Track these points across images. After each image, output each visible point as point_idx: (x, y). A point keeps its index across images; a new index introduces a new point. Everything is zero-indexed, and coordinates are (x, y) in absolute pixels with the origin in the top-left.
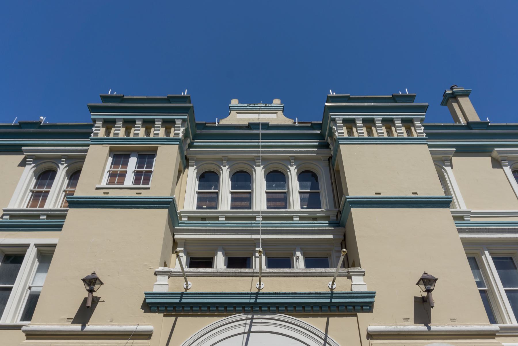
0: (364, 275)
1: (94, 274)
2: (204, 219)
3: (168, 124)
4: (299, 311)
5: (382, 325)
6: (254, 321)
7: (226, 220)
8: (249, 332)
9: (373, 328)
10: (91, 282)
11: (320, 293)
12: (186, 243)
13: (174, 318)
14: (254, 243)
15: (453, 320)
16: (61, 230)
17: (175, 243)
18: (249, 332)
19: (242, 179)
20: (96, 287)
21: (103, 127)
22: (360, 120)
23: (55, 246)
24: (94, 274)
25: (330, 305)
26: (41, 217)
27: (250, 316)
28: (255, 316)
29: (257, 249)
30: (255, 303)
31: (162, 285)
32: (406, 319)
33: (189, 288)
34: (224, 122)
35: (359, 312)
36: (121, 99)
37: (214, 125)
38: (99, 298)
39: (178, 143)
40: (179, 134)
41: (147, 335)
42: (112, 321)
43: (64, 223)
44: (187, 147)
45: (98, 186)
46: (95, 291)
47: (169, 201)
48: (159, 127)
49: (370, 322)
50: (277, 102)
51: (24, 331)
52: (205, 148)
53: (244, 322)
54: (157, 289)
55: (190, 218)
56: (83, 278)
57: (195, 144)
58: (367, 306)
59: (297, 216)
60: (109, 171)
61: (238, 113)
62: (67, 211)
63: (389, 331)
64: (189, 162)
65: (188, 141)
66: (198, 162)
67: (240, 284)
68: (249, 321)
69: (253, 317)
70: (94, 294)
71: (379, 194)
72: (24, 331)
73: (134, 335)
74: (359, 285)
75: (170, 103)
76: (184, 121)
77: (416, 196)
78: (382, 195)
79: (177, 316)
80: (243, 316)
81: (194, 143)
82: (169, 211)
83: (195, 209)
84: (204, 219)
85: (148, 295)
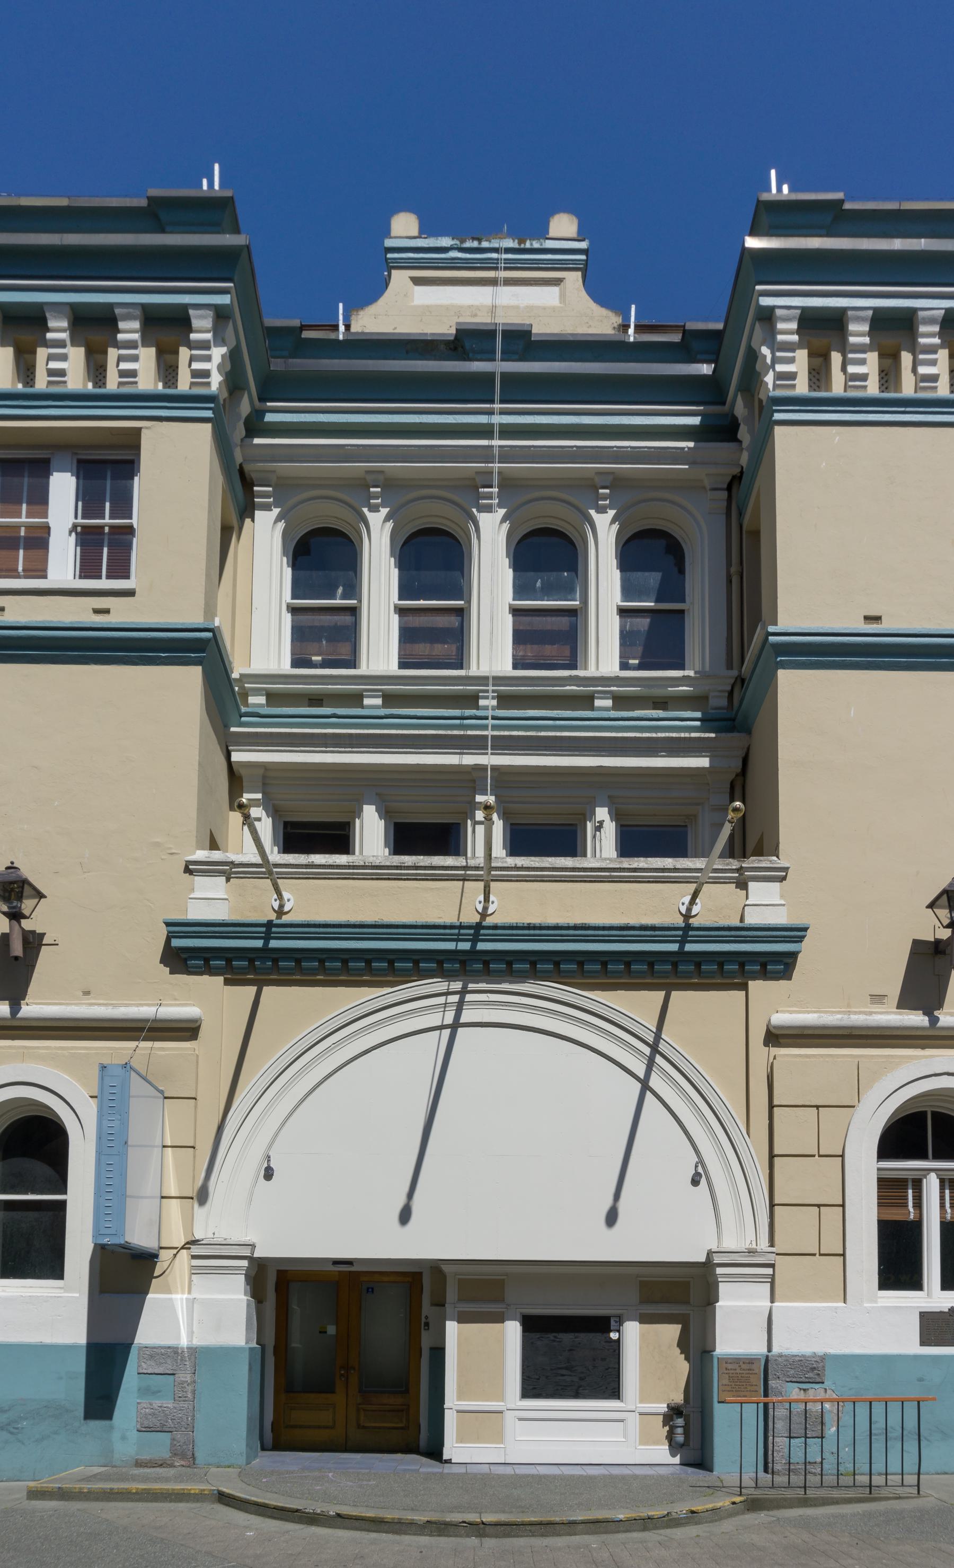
0: (783, 879)
2: (316, 700)
5: (808, 1012)
6: (469, 997)
7: (615, 707)
9: (782, 1018)
11: (653, 928)
12: (268, 777)
14: (471, 779)
20: (27, 905)
27: (457, 986)
28: (471, 986)
31: (211, 901)
32: (878, 999)
35: (754, 979)
36: (832, 218)
37: (331, 336)
41: (187, 1030)
42: (87, 993)
46: (25, 917)
53: (441, 1000)
54: (197, 912)
59: (257, 692)
66: (285, 490)
68: (456, 998)
73: (151, 1029)
74: (766, 905)
76: (221, 315)
78: (886, 626)
80: (440, 985)
84: (316, 700)
85: (176, 928)
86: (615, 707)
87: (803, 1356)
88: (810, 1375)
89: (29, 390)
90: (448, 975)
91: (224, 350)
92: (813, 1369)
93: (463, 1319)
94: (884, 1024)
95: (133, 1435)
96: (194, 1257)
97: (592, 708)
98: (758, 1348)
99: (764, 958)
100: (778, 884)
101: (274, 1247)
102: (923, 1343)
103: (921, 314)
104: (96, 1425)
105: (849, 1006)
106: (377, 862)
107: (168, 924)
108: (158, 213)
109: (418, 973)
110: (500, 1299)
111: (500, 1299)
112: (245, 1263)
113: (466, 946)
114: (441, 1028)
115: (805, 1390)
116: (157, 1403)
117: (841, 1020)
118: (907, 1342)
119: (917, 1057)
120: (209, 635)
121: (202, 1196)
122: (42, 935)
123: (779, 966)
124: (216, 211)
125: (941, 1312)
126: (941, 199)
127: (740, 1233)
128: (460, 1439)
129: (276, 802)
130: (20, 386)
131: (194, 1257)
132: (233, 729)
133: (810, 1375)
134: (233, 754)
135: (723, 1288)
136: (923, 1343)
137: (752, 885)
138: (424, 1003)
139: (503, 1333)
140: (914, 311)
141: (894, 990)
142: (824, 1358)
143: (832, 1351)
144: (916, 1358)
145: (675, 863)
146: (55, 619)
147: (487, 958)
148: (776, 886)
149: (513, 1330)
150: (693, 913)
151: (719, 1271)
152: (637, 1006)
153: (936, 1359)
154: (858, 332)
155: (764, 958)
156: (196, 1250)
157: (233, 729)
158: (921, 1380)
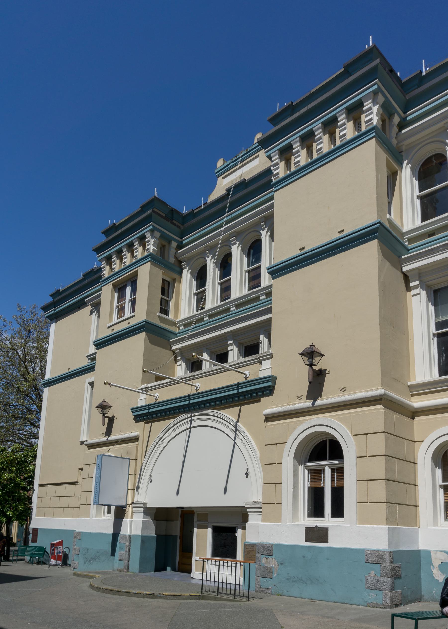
0: (272, 357)
1: (312, 346)
2: (431, 234)
3: (355, 112)
4: (218, 405)
5: (273, 408)
6: (193, 418)
7: (237, 308)
8: (190, 428)
9: (268, 411)
10: (311, 354)
11: (229, 386)
12: (420, 273)
13: (239, 407)
14: (225, 337)
15: (343, 390)
16: (94, 370)
17: (407, 278)
18: (190, 428)
19: (225, 266)
20: (316, 360)
21: (348, 121)
22: (297, 142)
23: (93, 384)
24: (312, 346)
25: (238, 395)
26: (231, 309)
27: (189, 415)
28: (193, 414)
29: (229, 342)
30: (189, 404)
31: (142, 400)
32: (299, 397)
33: (247, 377)
34: (213, 197)
35: (262, 397)
36: (292, 108)
37: (200, 208)
38: (326, 370)
39: (374, 134)
40: (371, 119)
41: (135, 439)
42: (121, 431)
43: (96, 364)
44: (396, 129)
45: (109, 325)
46: (315, 365)
47: (142, 325)
48: (298, 151)
49: (268, 405)
50: (220, 163)
51: (86, 445)
52: (195, 241)
53: (186, 421)
54: (141, 403)
55: (210, 316)
56: (300, 352)
57: (184, 242)
58: (267, 390)
59: (262, 295)
60: (118, 307)
61: (224, 178)
62: (95, 353)
63: (279, 413)
64: (181, 266)
65: (396, 119)
66: (188, 261)
67: (227, 379)
68: (189, 419)
69: (191, 415)
70: (315, 368)
71: (303, 248)
72: (86, 445)
73: (122, 441)
74: (265, 369)
75: (351, 75)
76: (152, 231)
77: (303, 252)
78: (306, 249)
79: (241, 405)
80: (185, 416)
81: (182, 242)
82: (380, 241)
83: (418, 222)
84: (431, 234)
85: (134, 410)
86: (237, 308)
87: (266, 544)
88: (268, 552)
89: (361, 133)
90: (187, 412)
91: (377, 106)
92: (269, 550)
93: (198, 527)
94: (297, 408)
95: (118, 561)
96: (133, 507)
97: (204, 321)
98: (128, 533)
99: (262, 390)
100: (270, 360)
101: (152, 504)
102: (306, 540)
103: (314, 129)
104: (112, 557)
105: (290, 402)
106: (208, 370)
107: (131, 409)
108: (349, 70)
109: (180, 413)
110: (206, 521)
111: (206, 521)
112: (142, 509)
113: (187, 402)
114: (187, 429)
115: (267, 558)
116: (122, 552)
117: (283, 409)
118: (299, 539)
119: (307, 420)
120: (379, 224)
121: (138, 489)
122: (326, 370)
123: (268, 391)
124: (373, 52)
125: (312, 527)
126: (330, 77)
127: (256, 496)
128: (196, 571)
129: (427, 283)
130: (357, 133)
131: (133, 507)
132: (403, 257)
133: (268, 552)
134: (403, 268)
135: (250, 517)
136: (306, 540)
137: (263, 362)
138: (182, 421)
139: (207, 532)
140: (312, 129)
141: (305, 392)
142: (273, 545)
143: (276, 542)
144: (302, 547)
145: (253, 357)
146: (321, 244)
147: (262, 390)
148: (269, 361)
149: (209, 531)
150: (247, 377)
151: (248, 510)
152: (230, 414)
153: (309, 547)
154: (297, 146)
155: (262, 390)
156: (134, 505)
157: (403, 257)
158: (304, 557)
